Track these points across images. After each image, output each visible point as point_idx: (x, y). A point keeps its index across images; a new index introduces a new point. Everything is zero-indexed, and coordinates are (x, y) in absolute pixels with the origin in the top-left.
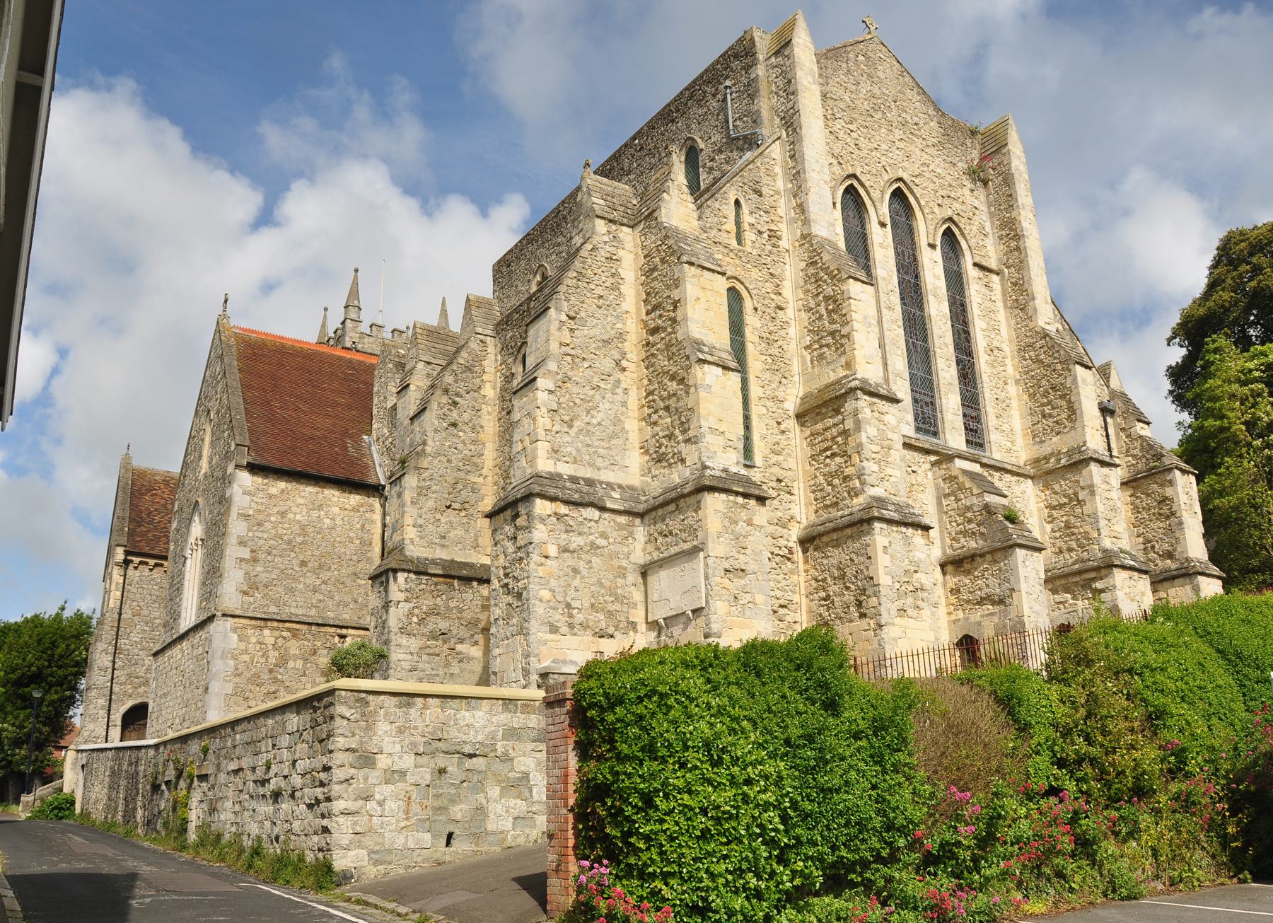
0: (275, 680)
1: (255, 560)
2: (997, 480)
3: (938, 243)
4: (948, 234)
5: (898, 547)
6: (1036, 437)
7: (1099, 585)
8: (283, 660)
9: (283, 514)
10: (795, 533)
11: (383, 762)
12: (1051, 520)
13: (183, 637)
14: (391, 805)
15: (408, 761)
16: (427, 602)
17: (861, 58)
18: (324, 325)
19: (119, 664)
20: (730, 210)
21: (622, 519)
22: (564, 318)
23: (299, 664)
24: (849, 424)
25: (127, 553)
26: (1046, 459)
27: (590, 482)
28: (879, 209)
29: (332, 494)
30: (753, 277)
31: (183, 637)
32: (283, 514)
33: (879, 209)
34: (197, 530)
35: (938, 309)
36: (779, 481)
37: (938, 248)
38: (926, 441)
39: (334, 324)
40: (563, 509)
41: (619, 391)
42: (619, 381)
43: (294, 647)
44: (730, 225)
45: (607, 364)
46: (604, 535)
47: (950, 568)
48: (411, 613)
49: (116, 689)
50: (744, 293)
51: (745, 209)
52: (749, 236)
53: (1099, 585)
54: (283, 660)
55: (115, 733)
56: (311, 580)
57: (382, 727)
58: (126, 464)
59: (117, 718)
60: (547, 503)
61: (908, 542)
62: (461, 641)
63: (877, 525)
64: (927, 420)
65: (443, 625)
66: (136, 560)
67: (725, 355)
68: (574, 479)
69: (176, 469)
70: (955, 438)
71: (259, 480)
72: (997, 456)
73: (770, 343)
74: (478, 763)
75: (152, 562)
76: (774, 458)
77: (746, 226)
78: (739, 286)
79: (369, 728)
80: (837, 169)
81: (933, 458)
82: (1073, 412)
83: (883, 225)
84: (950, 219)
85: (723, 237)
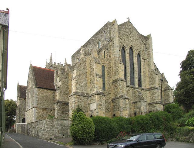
0: (43, 116)
1: (38, 100)
2: (143, 92)
3: (137, 56)
4: (139, 54)
5: (124, 101)
6: (149, 85)
7: (155, 106)
8: (43, 113)
9: (42, 94)
10: (111, 99)
11: (55, 127)
12: (150, 97)
13: (29, 110)
14: (56, 131)
15: (58, 127)
16: (62, 107)
17: (127, 25)
18: (47, 62)
19: (20, 113)
20: (103, 53)
21: (86, 98)
22: (78, 70)
23: (46, 114)
24: (118, 85)
25: (20, 98)
26: (150, 88)
27: (82, 93)
28: (128, 51)
29: (49, 91)
30: (106, 63)
31: (29, 110)
32: (42, 94)
33: (128, 51)
34: (30, 95)
35: (136, 66)
36: (109, 92)
37: (137, 57)
38: (133, 86)
39: (48, 62)
40: (78, 96)
41: (86, 80)
42: (86, 79)
43: (45, 112)
44: (103, 55)
45: (84, 77)
46: (84, 100)
47: (134, 104)
48: (60, 108)
49: (21, 116)
50: (105, 66)
51: (106, 53)
52: (106, 57)
53: (155, 106)
54: (43, 113)
55: (21, 122)
56: (46, 103)
57: (55, 123)
58: (18, 85)
59: (21, 120)
60: (76, 96)
61: (125, 101)
62: (67, 112)
63: (121, 99)
64: (133, 83)
65: (64, 110)
66: (21, 99)
67: (101, 76)
68: (80, 92)
69: (26, 85)
70: (137, 85)
71: (38, 89)
72: (143, 88)
73: (109, 73)
74: (67, 127)
75: (24, 99)
76: (108, 89)
77: (106, 55)
78: (104, 65)
79: (53, 123)
80: (121, 45)
81: (132, 88)
82: (154, 81)
83: (128, 53)
84: (139, 52)
85: (102, 57)
